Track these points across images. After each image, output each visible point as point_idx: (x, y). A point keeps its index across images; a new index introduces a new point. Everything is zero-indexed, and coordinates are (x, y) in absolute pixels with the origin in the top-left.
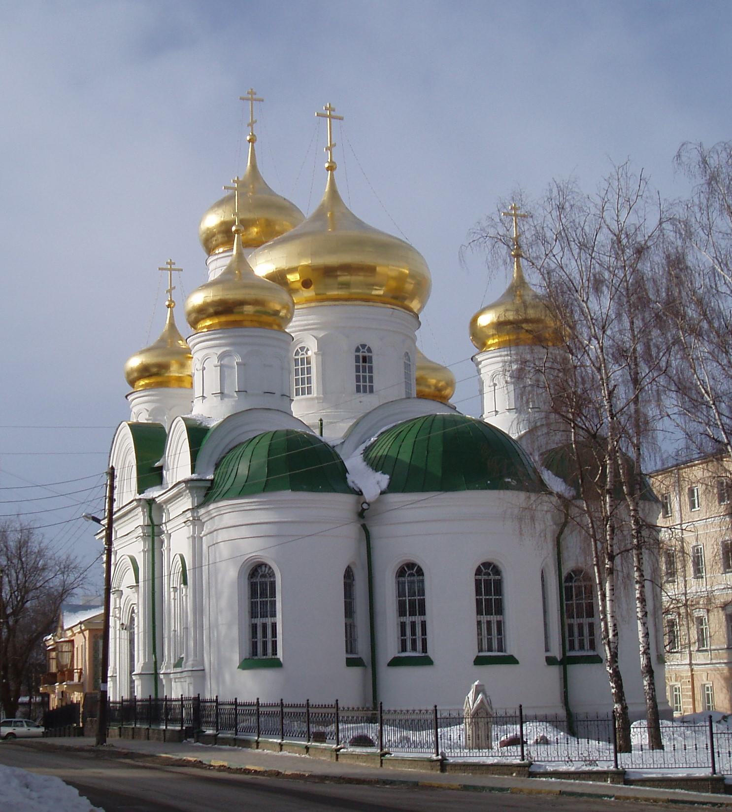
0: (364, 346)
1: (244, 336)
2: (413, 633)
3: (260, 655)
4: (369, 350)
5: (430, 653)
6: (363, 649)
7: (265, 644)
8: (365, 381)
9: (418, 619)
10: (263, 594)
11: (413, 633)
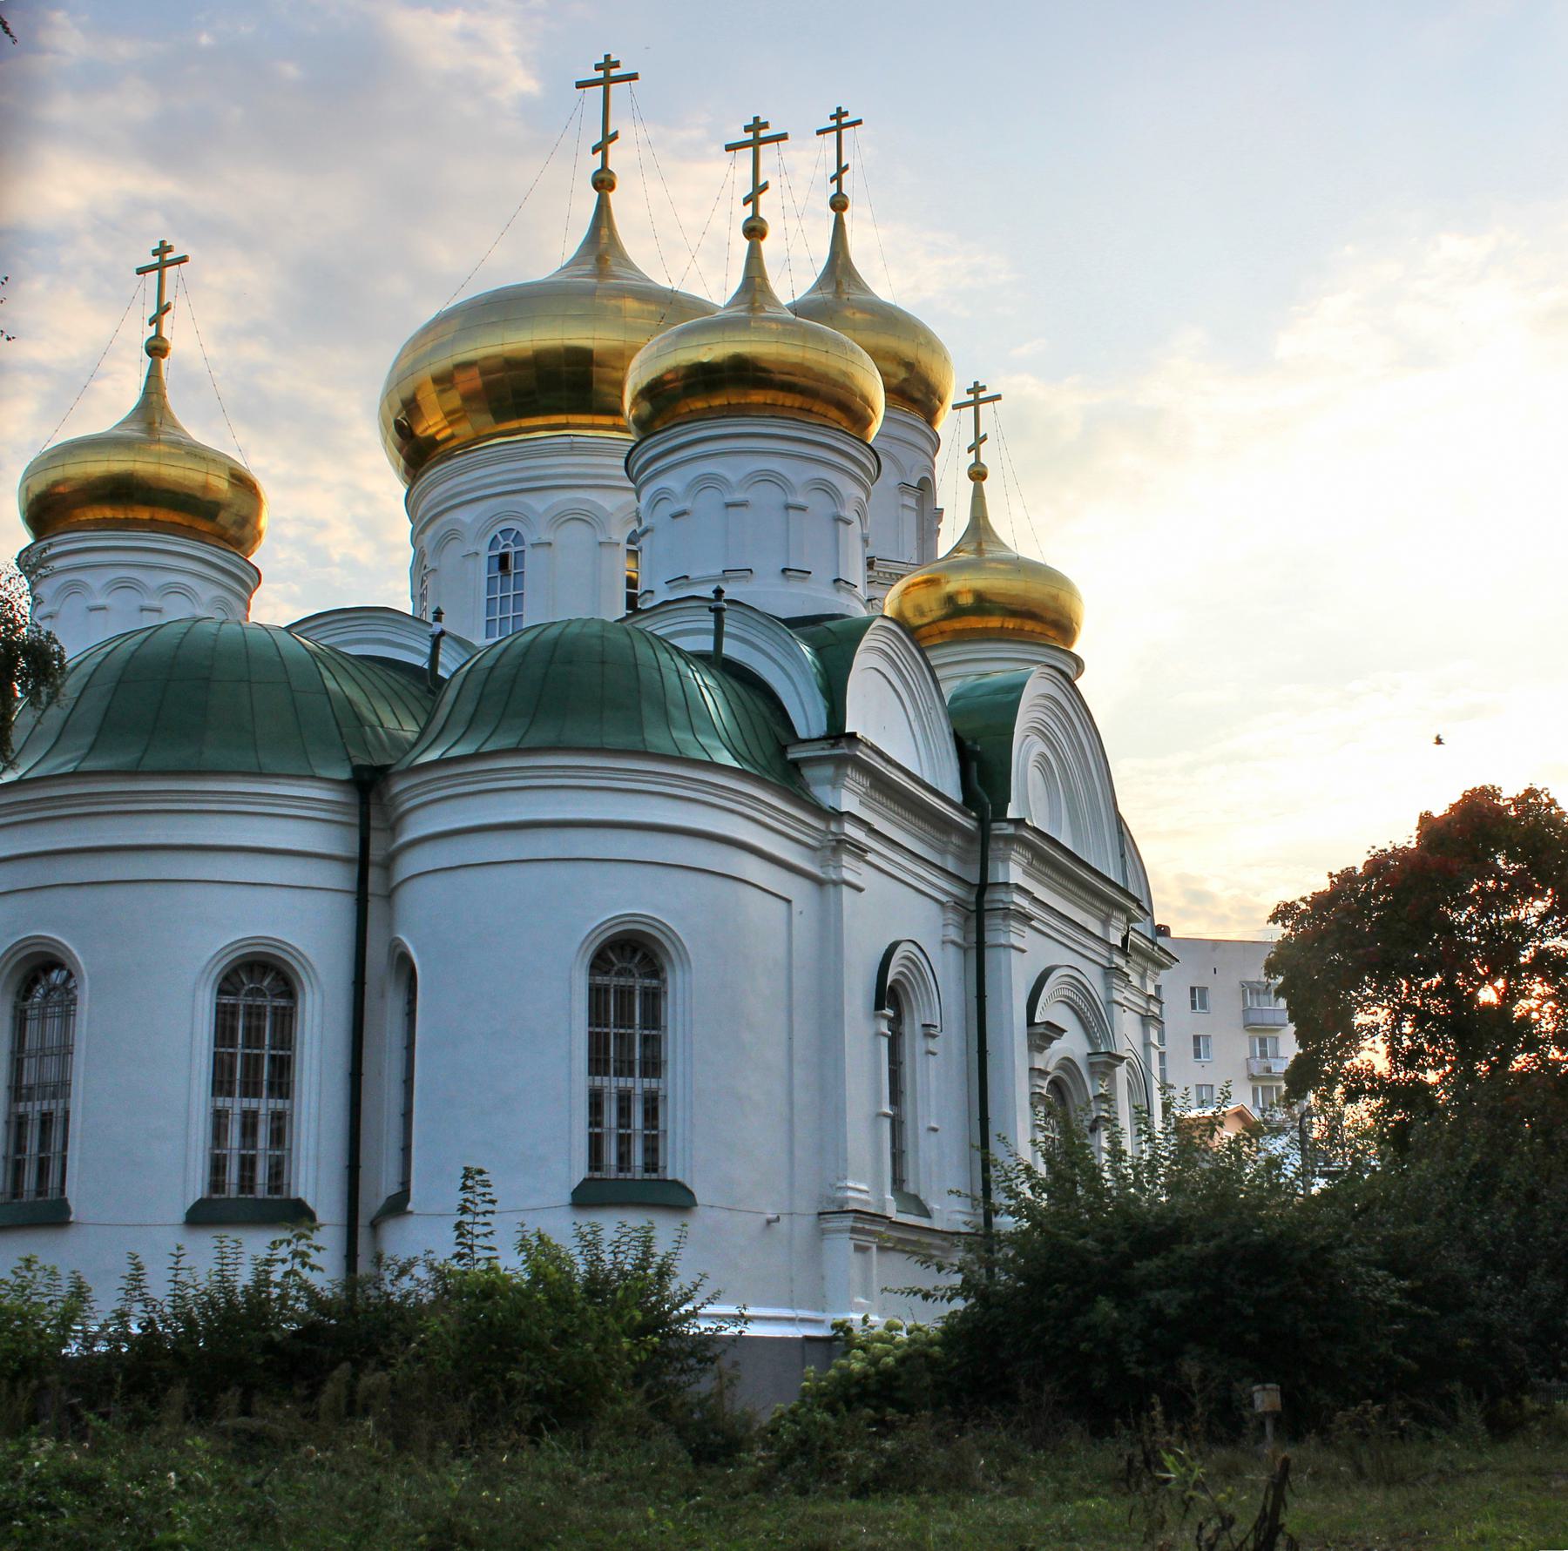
7: (624, 1141)
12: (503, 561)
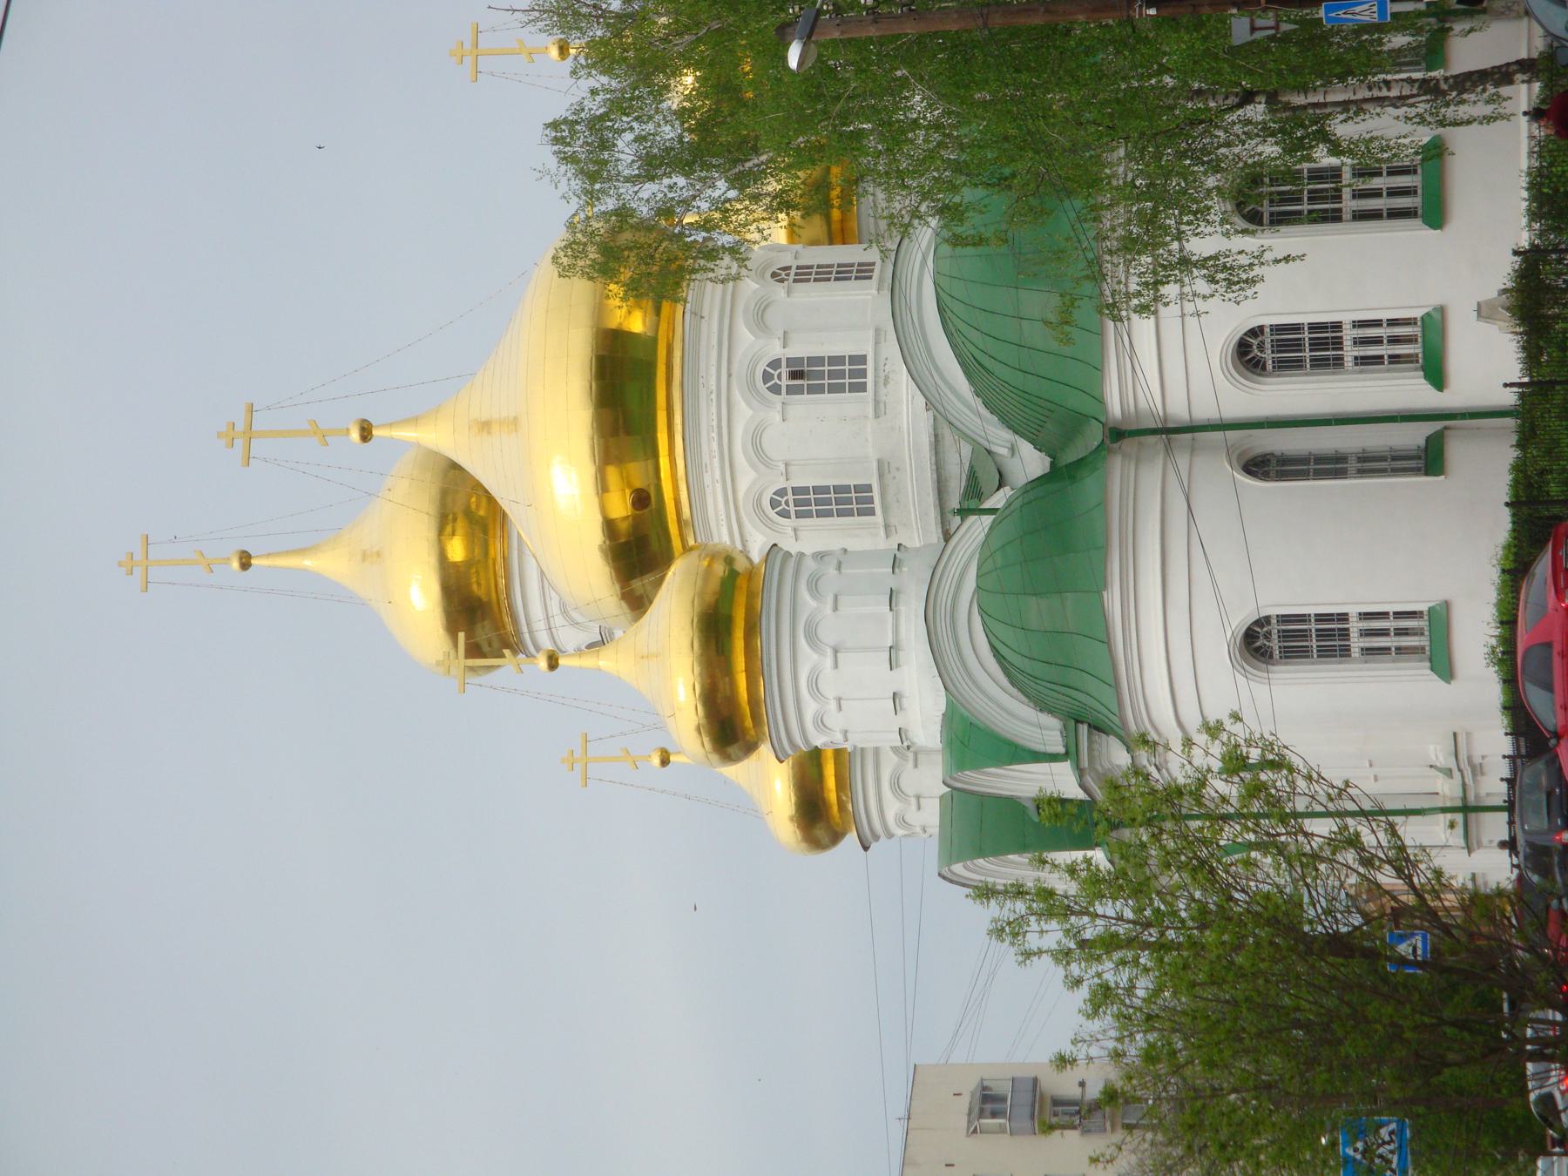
0: (767, 377)
1: (781, 574)
3: (1423, 641)
4: (775, 364)
5: (1417, 313)
6: (1412, 436)
7: (1401, 632)
8: (841, 374)
9: (1348, 334)
10: (1297, 345)
12: (795, 375)
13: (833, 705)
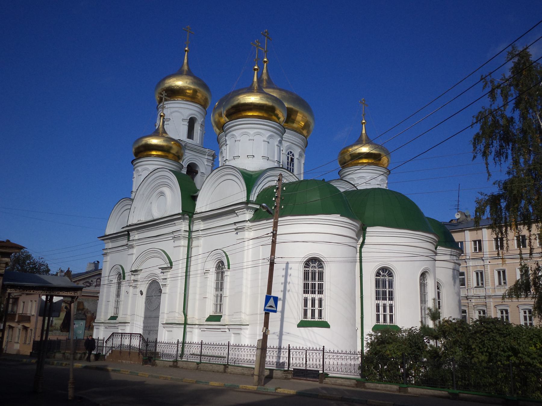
2: (385, 311)
11: (385, 311)
13: (251, 138)
